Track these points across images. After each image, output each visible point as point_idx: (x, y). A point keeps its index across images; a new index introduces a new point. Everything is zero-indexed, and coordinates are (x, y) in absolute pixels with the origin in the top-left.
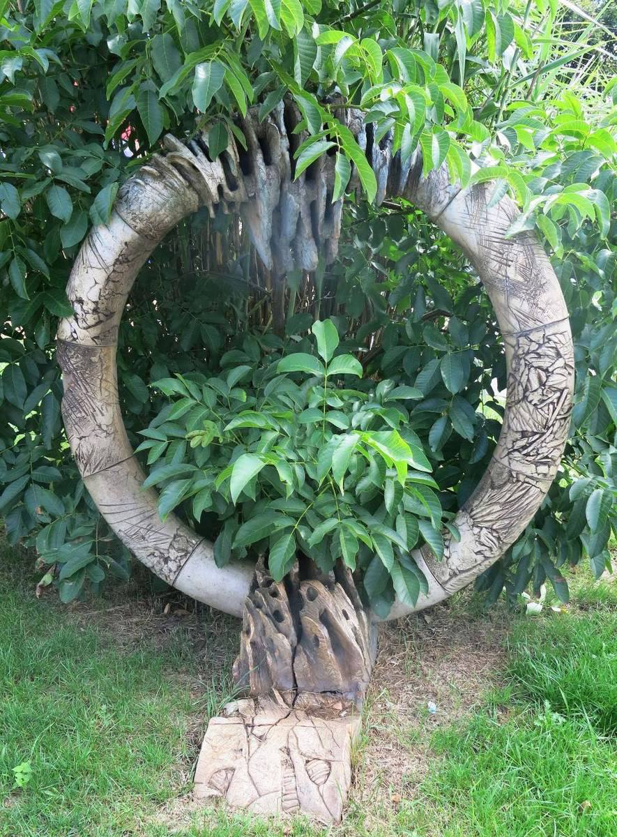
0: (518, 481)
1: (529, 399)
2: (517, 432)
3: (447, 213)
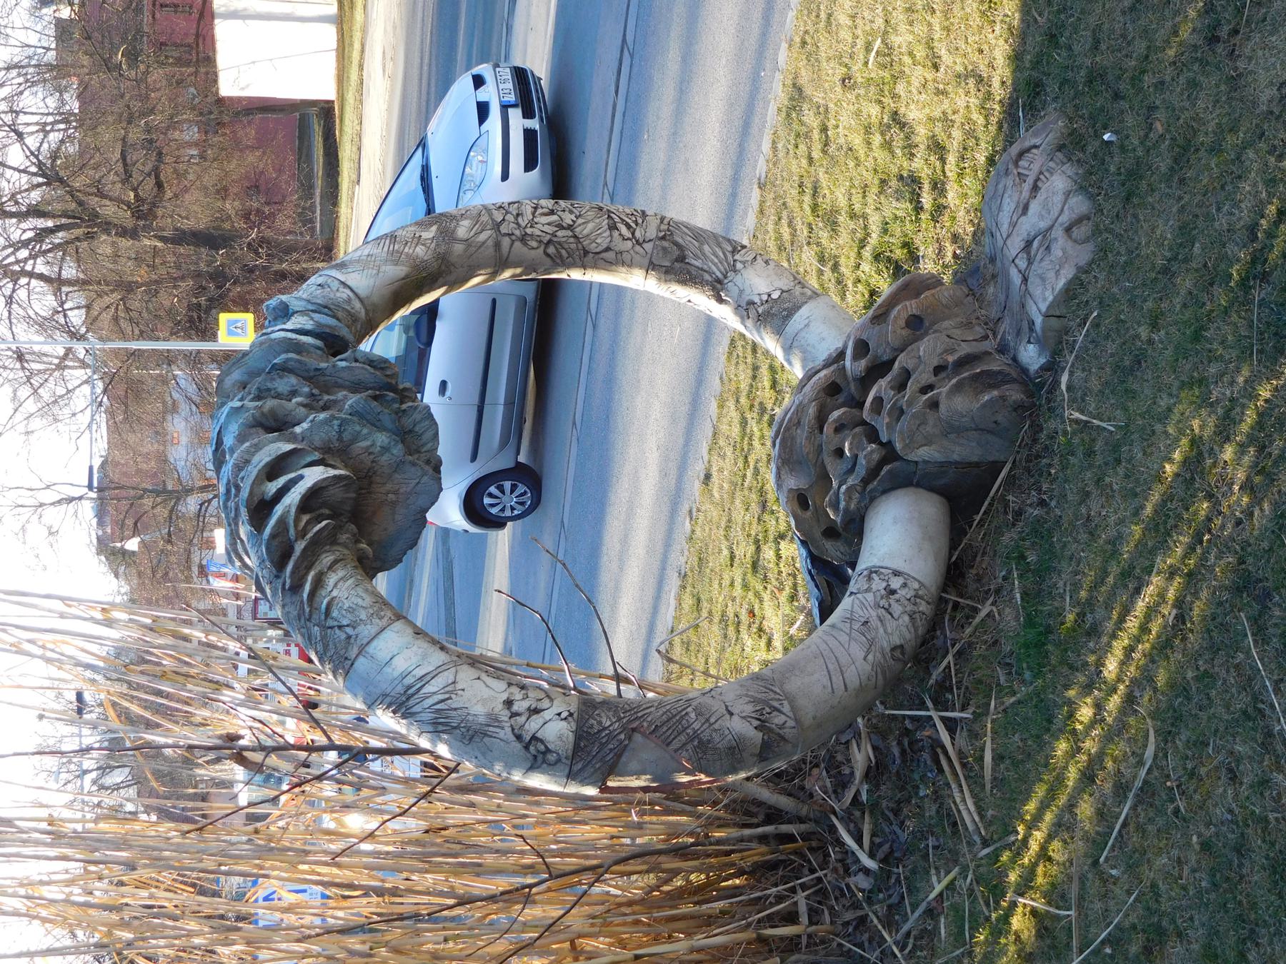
0: (669, 230)
1: (571, 223)
2: (611, 236)
3: (362, 293)
